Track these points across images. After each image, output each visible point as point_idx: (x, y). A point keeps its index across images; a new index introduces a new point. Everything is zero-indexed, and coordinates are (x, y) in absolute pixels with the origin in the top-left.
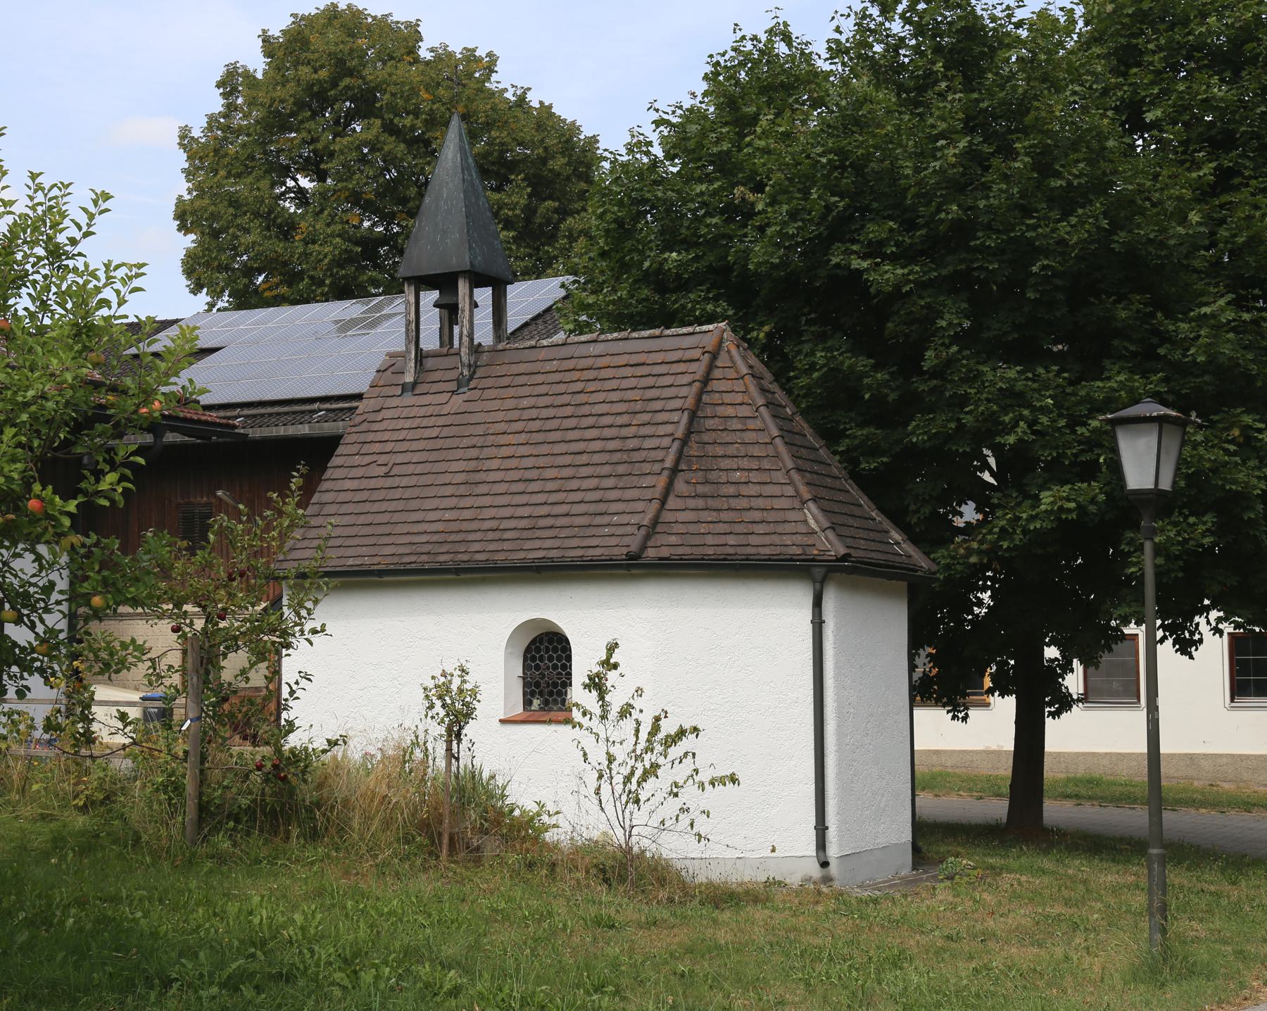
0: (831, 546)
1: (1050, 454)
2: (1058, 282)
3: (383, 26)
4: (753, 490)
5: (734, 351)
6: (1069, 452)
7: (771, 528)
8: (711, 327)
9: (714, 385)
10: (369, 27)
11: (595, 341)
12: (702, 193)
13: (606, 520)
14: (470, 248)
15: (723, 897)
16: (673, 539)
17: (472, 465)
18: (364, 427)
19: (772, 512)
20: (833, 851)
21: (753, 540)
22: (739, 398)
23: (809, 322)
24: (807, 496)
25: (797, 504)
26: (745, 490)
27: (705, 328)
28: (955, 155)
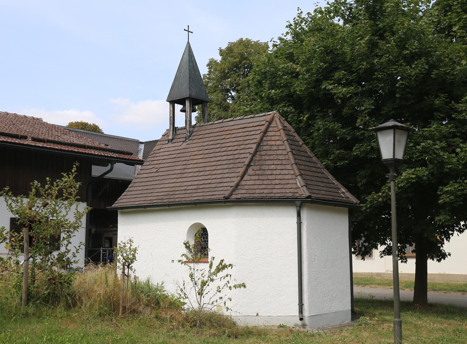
0: (305, 193)
1: (407, 157)
2: (408, 90)
3: (257, 44)
4: (278, 172)
5: (278, 121)
6: (414, 156)
7: (282, 186)
8: (271, 113)
9: (269, 134)
10: (252, 45)
11: (232, 120)
12: (283, 68)
13: (222, 185)
14: (190, 89)
15: (249, 332)
16: (244, 191)
17: (184, 167)
18: (153, 155)
19: (284, 180)
20: (306, 314)
21: (274, 191)
22: (277, 138)
23: (317, 112)
24: (298, 174)
25: (294, 177)
26: (274, 172)
27: (269, 113)
28: (364, 43)
